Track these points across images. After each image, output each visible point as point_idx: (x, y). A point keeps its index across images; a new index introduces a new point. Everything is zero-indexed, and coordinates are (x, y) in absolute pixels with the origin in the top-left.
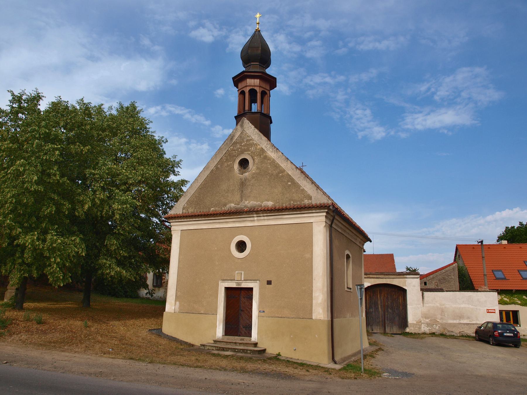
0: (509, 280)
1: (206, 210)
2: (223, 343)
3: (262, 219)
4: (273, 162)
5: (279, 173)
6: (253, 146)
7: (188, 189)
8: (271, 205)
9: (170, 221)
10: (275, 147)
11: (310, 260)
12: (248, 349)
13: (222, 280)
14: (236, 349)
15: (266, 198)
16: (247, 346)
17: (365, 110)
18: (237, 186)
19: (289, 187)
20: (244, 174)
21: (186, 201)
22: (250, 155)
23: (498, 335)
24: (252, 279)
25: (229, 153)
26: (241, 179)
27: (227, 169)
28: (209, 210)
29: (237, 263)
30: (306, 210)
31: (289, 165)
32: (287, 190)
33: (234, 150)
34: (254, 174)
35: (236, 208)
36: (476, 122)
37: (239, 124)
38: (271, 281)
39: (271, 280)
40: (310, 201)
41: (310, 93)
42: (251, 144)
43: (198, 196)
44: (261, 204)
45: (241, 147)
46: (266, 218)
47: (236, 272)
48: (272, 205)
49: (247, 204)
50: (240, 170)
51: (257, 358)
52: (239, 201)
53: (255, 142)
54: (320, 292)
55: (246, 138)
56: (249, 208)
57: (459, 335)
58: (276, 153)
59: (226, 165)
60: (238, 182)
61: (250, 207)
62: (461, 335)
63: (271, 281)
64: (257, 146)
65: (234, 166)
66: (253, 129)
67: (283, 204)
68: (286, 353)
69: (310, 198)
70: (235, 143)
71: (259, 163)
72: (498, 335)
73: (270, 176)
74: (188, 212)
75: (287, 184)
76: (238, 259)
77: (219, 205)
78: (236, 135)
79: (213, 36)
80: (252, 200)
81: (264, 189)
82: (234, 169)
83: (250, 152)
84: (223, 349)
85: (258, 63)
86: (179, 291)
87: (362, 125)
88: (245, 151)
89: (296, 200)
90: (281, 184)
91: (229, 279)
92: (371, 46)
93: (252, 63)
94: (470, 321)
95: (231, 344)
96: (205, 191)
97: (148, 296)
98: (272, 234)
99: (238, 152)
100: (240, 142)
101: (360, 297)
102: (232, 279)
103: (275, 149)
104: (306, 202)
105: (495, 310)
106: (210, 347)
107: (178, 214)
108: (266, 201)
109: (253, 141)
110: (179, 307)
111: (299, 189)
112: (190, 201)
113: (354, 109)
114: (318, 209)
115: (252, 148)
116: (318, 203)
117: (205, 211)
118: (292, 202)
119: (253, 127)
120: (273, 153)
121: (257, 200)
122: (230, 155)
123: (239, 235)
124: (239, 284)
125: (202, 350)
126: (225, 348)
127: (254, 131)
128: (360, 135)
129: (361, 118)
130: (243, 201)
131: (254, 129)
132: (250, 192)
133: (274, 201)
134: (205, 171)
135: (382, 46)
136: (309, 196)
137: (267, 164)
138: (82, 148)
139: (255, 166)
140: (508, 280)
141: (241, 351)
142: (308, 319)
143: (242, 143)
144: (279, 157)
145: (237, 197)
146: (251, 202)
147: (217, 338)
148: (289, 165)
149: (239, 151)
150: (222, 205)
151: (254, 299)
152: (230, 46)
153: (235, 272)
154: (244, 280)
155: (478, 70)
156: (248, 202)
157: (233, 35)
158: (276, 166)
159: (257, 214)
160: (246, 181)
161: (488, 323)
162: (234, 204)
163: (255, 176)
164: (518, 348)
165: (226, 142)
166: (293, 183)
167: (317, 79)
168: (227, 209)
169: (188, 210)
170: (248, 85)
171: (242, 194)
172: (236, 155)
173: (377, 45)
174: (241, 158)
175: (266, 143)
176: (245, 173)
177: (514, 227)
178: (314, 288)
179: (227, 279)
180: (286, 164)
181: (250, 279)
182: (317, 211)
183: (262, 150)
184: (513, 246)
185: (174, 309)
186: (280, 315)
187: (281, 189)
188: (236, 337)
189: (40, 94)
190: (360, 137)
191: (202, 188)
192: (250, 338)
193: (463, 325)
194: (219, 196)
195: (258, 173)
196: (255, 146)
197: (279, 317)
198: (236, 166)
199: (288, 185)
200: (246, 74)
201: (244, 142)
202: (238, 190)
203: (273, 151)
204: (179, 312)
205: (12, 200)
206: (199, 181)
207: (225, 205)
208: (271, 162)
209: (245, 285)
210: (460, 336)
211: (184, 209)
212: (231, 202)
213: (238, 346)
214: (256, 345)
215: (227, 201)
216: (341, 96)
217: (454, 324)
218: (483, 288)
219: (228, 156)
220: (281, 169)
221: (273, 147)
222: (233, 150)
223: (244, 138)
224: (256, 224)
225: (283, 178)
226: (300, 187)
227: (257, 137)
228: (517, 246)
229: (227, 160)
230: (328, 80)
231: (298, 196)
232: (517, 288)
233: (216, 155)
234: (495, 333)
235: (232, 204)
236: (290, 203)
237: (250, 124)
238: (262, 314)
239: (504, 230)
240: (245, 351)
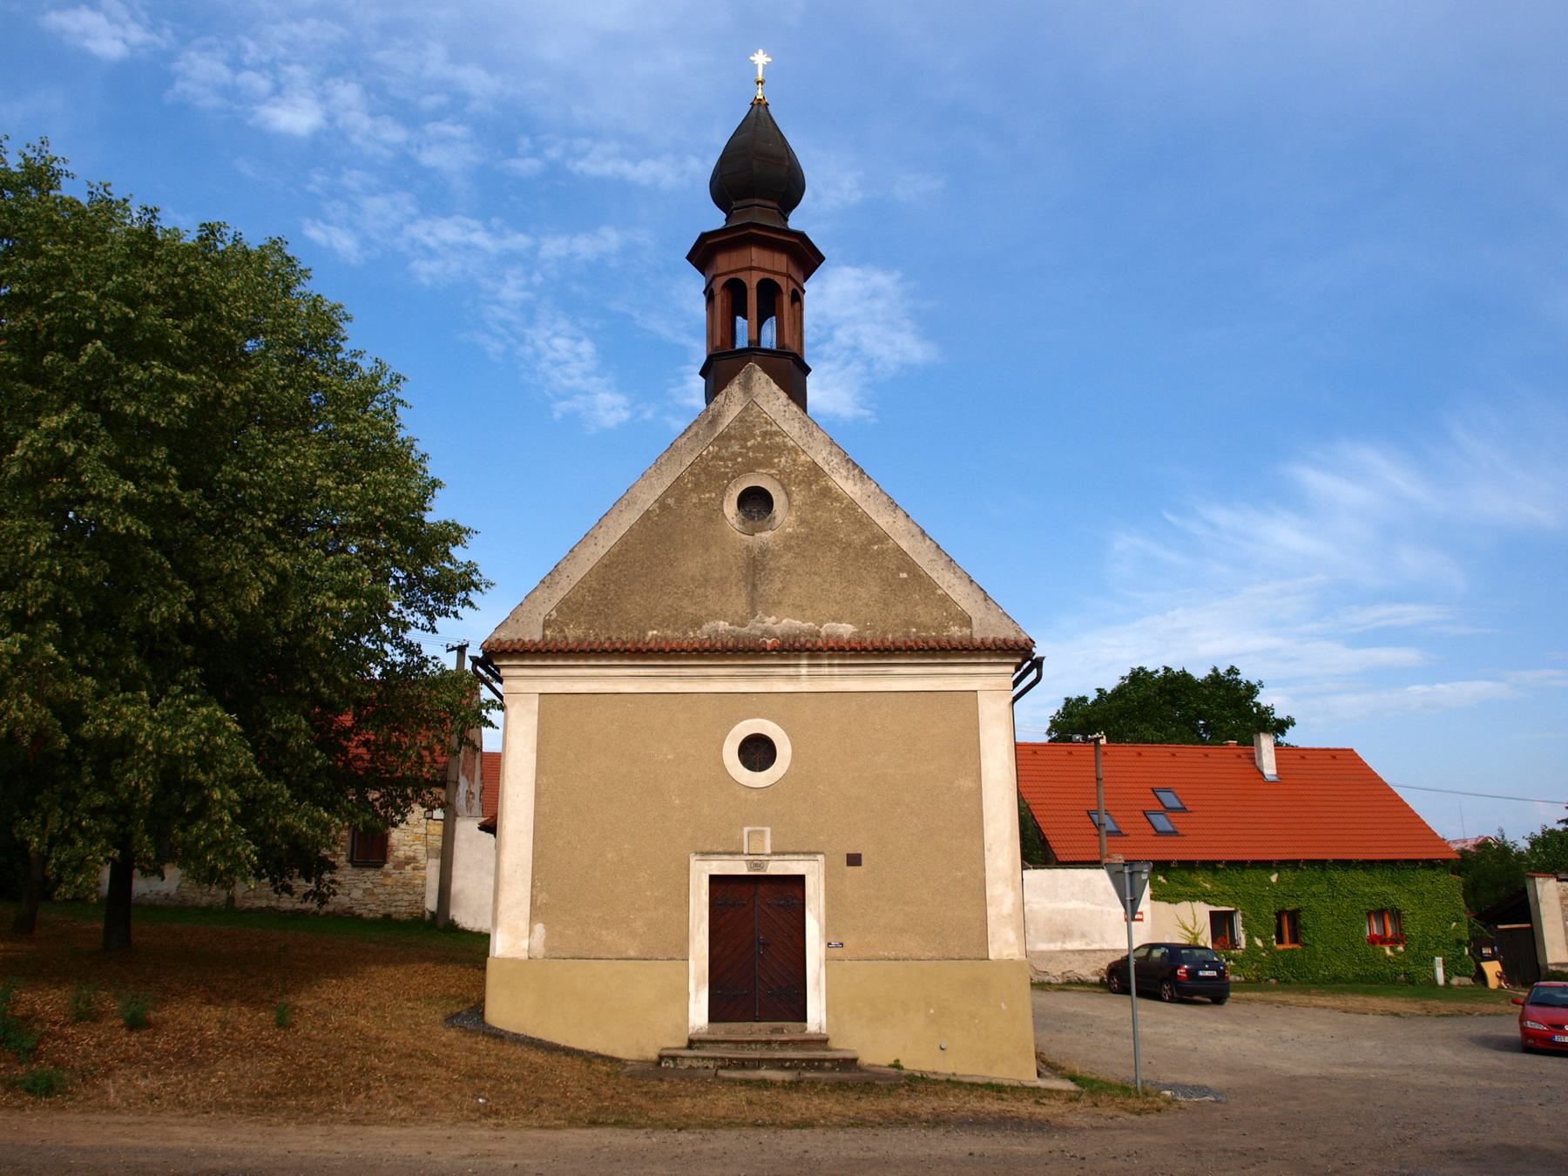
2: (725, 1045)
5: (871, 542)
6: (786, 452)
9: (500, 661)
13: (696, 853)
14: (825, 1060)
16: (808, 1050)
17: (578, 340)
20: (757, 535)
21: (555, 602)
24: (797, 850)
27: (700, 513)
31: (902, 522)
32: (896, 595)
33: (722, 459)
34: (790, 536)
36: (867, 413)
38: (860, 855)
40: (967, 631)
41: (425, 270)
42: (779, 448)
43: (597, 587)
45: (745, 451)
46: (836, 670)
47: (746, 830)
48: (853, 633)
56: (778, 638)
57: (1060, 981)
58: (859, 484)
59: (694, 501)
61: (782, 636)
63: (860, 855)
64: (797, 454)
65: (725, 505)
66: (785, 403)
67: (885, 632)
68: (918, 1060)
69: (967, 622)
70: (725, 438)
73: (844, 549)
74: (566, 638)
79: (124, 41)
80: (788, 616)
81: (827, 585)
82: (724, 515)
83: (773, 471)
84: (743, 1064)
87: (566, 382)
88: (760, 464)
89: (925, 623)
90: (877, 576)
91: (720, 849)
93: (757, 201)
95: (753, 1046)
97: (312, 905)
102: (733, 849)
103: (856, 471)
104: (956, 632)
105: (1279, 915)
107: (527, 639)
108: (833, 621)
111: (934, 594)
113: (548, 333)
114: (998, 656)
115: (783, 460)
117: (627, 636)
118: (914, 630)
119: (783, 395)
120: (851, 482)
124: (757, 865)
125: (662, 1066)
137: (830, 511)
138: (220, 385)
140: (1126, 835)
142: (975, 959)
143: (746, 440)
146: (785, 621)
147: (690, 1031)
150: (686, 623)
152: (179, 86)
154: (774, 853)
155: (881, 280)
156: (773, 619)
157: (193, 55)
158: (864, 522)
159: (810, 657)
160: (764, 556)
161: (1152, 946)
163: (793, 543)
165: (695, 429)
167: (448, 231)
169: (562, 631)
170: (754, 264)
172: (730, 475)
175: (828, 449)
177: (1084, 699)
178: (989, 875)
180: (891, 520)
181: (791, 849)
183: (815, 471)
187: (877, 589)
188: (757, 1025)
189: (55, 164)
190: (557, 415)
191: (613, 563)
193: (1070, 954)
194: (676, 593)
196: (789, 453)
198: (730, 508)
199: (901, 579)
200: (754, 231)
203: (851, 476)
204: (545, 957)
205: (51, 566)
207: (697, 624)
209: (776, 868)
211: (549, 626)
212: (717, 616)
213: (777, 1051)
214: (822, 1042)
216: (512, 290)
221: (850, 465)
222: (717, 457)
223: (754, 426)
224: (805, 686)
225: (884, 558)
227: (797, 430)
229: (697, 484)
233: (658, 465)
235: (722, 623)
237: (775, 387)
238: (838, 952)
239: (1060, 706)
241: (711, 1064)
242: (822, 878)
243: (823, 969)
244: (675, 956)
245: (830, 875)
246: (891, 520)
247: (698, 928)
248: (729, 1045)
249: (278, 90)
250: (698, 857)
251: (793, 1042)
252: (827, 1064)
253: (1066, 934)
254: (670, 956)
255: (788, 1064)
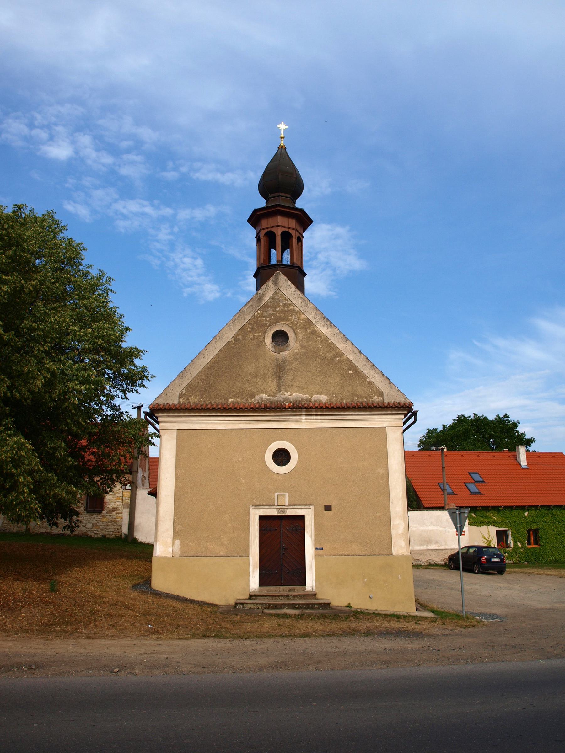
0: (484, 494)
1: (220, 401)
3: (313, 419)
4: (325, 340)
7: (186, 367)
8: (325, 399)
9: (158, 413)
10: (328, 320)
11: (386, 477)
12: (316, 603)
13: (253, 505)
15: (317, 390)
17: (195, 259)
18: (270, 369)
19: (350, 377)
20: (281, 353)
21: (184, 385)
22: (291, 327)
23: (485, 561)
24: (301, 504)
25: (255, 320)
26: (277, 360)
27: (254, 343)
28: (226, 401)
29: (276, 480)
30: (379, 411)
31: (350, 347)
33: (264, 317)
34: (297, 354)
35: (271, 400)
37: (272, 280)
39: (331, 504)
41: (121, 224)
42: (291, 312)
43: (205, 378)
44: (310, 397)
45: (275, 313)
46: (319, 417)
47: (276, 494)
48: (327, 400)
49: (288, 396)
50: (274, 346)
51: (346, 614)
52: (275, 391)
53: (298, 309)
54: (401, 520)
55: (284, 302)
56: (291, 402)
57: (426, 564)
58: (330, 329)
60: (272, 364)
61: (293, 401)
62: (428, 564)
63: (331, 506)
64: (300, 315)
65: (266, 339)
67: (342, 399)
69: (382, 394)
70: (266, 307)
71: (305, 340)
72: (485, 561)
73: (322, 359)
74: (189, 403)
75: (348, 373)
76: (277, 475)
77: (243, 395)
78: (267, 295)
83: (289, 323)
84: (276, 606)
85: (289, 196)
86: (178, 524)
88: (283, 319)
91: (264, 503)
92: (210, 177)
93: (281, 194)
94: (438, 546)
95: (280, 598)
96: (218, 373)
98: (328, 441)
99: (271, 320)
100: (273, 305)
101: (460, 524)
102: (270, 503)
103: (328, 323)
104: (376, 399)
105: (529, 531)
106: (252, 605)
108: (318, 394)
109: (294, 306)
110: (181, 547)
112: (192, 386)
113: (181, 256)
114: (396, 410)
116: (393, 401)
117: (219, 402)
118: (356, 398)
120: (326, 328)
121: (303, 391)
122: (256, 322)
123: (277, 440)
126: (278, 604)
127: (295, 293)
128: (187, 291)
129: (189, 270)
130: (281, 392)
131: (296, 291)
132: (292, 379)
133: (330, 395)
134: (216, 342)
135: (226, 178)
136: (380, 392)
137: (316, 342)
139: (299, 343)
141: (305, 606)
143: (276, 308)
144: (334, 335)
145: (272, 385)
146: (294, 394)
147: (250, 591)
148: (349, 347)
149: (272, 319)
151: (307, 532)
153: (274, 493)
154: (290, 505)
156: (289, 393)
158: (332, 347)
159: (307, 411)
160: (284, 363)
161: (469, 547)
162: (267, 395)
163: (298, 357)
164: (502, 574)
165: (251, 303)
166: (356, 372)
167: (133, 206)
168: (257, 402)
169: (188, 399)
170: (279, 224)
171: (280, 382)
172: (268, 325)
173: (219, 176)
174: (275, 330)
176: (283, 351)
179: (261, 504)
180: (345, 346)
181: (298, 503)
182: (393, 413)
183: (309, 322)
184: (454, 453)
185: (171, 552)
186: (347, 552)
187: (338, 379)
190: (185, 295)
192: (304, 587)
194: (243, 381)
195: (303, 353)
197: (345, 556)
198: (268, 340)
200: (279, 208)
201: (280, 307)
202: (273, 375)
203: (326, 325)
204: (180, 556)
206: (206, 357)
207: (253, 395)
208: (322, 341)
209: (291, 512)
210: (428, 565)
211: (182, 397)
212: (262, 392)
213: (292, 600)
215: (256, 390)
216: (164, 235)
217: (421, 550)
218: (451, 506)
219: (253, 324)
220: (337, 351)
221: (325, 320)
222: (262, 316)
223: (280, 301)
224: (304, 425)
226: (366, 378)
228: (458, 453)
229: (252, 329)
230: (148, 210)
231: (364, 390)
232: (492, 504)
234: (482, 559)
235: (264, 395)
236: (353, 399)
237: (289, 283)
238: (320, 552)
240: (311, 606)
241: (260, 607)
242: (313, 517)
243: (314, 560)
244: (243, 555)
245: (317, 516)
246: (345, 346)
247: (254, 541)
248: (269, 598)
249: (52, 138)
250: (253, 507)
251: (299, 595)
252: (316, 606)
253: (429, 542)
254: (241, 555)
255: (297, 606)
